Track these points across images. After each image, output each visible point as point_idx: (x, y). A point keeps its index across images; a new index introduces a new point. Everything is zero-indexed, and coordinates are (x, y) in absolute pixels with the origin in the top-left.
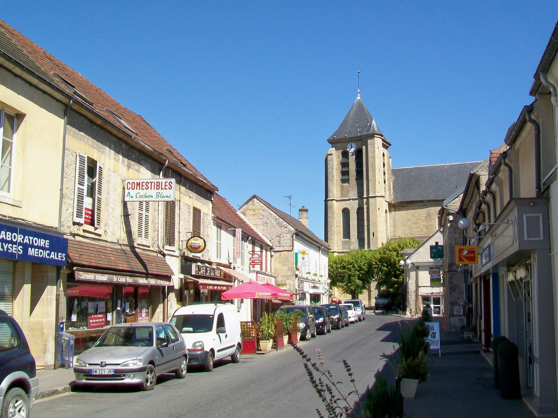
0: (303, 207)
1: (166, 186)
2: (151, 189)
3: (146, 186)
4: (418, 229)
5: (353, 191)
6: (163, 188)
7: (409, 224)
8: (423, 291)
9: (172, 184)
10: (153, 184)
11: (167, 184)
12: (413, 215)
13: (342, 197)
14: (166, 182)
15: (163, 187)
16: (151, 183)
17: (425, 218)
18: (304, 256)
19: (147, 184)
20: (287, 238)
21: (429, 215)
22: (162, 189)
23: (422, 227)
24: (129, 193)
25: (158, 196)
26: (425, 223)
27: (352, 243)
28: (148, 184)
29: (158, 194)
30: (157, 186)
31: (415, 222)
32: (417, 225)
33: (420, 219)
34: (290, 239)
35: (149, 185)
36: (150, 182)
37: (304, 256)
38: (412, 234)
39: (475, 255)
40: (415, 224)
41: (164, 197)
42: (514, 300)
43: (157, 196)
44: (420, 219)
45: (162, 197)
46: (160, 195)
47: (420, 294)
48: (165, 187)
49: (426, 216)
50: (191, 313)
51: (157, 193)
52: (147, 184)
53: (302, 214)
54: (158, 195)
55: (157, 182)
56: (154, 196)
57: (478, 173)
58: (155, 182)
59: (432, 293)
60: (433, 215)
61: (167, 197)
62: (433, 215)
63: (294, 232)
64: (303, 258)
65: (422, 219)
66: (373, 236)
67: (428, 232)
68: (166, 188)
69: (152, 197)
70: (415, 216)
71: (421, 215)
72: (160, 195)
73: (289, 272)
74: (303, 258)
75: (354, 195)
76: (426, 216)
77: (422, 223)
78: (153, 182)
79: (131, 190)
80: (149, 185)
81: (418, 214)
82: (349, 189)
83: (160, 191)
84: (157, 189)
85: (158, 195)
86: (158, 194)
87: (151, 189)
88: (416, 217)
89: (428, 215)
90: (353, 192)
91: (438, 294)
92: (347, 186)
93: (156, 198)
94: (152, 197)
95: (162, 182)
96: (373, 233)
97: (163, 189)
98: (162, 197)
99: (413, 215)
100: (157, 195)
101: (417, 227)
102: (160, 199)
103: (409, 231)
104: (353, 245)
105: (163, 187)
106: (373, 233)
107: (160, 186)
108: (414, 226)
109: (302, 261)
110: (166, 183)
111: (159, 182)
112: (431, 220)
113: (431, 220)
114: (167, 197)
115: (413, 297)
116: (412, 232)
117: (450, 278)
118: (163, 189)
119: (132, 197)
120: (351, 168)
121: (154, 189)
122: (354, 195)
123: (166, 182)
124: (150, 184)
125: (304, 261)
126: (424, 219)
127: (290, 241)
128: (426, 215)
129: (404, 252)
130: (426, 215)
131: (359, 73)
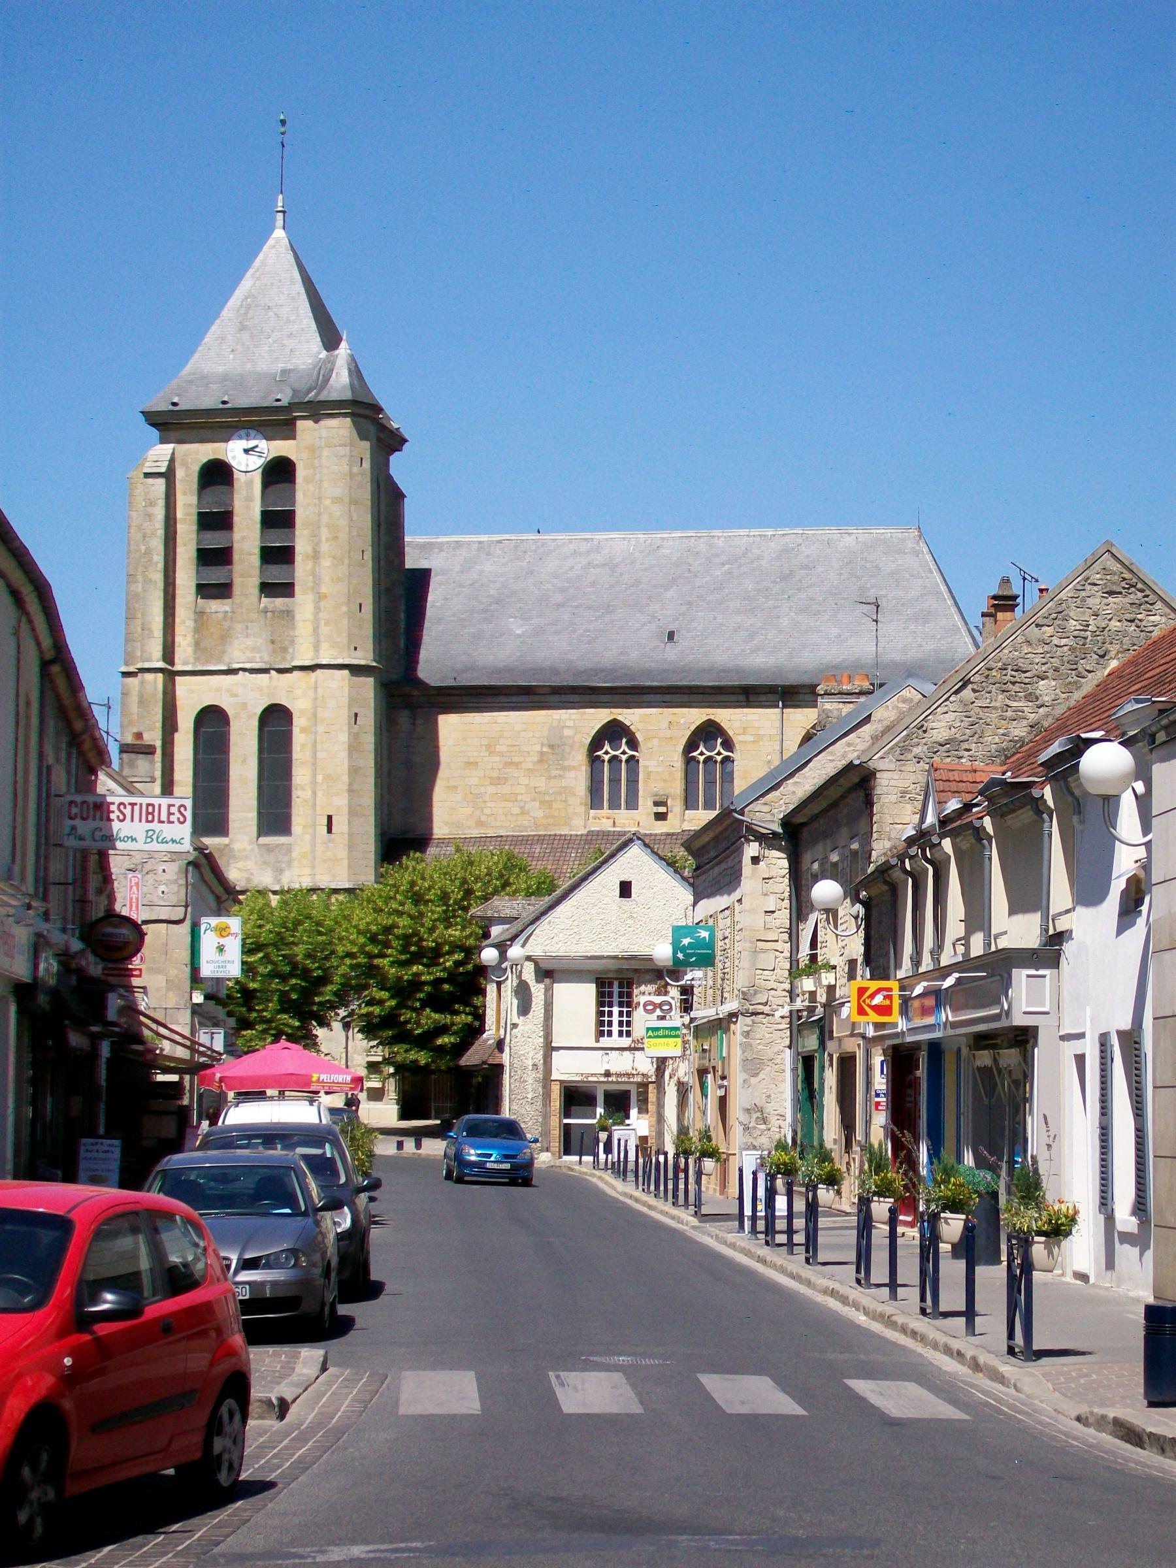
0: (139, 735)
1: (170, 814)
2: (132, 820)
3: (119, 814)
4: (509, 804)
5: (247, 636)
6: (162, 819)
7: (474, 781)
8: (568, 1068)
9: (186, 809)
10: (137, 808)
11: (173, 810)
12: (488, 746)
13: (197, 659)
14: (170, 806)
15: (164, 817)
16: (133, 805)
17: (541, 761)
18: (222, 941)
19: (122, 807)
20: (165, 877)
21: (556, 746)
22: (160, 822)
23: (526, 798)
24: (74, 828)
25: (149, 837)
26: (540, 783)
27: (234, 857)
28: (125, 808)
29: (151, 833)
30: (148, 813)
31: (495, 774)
32: (505, 789)
33: (516, 765)
34: (175, 881)
35: (128, 811)
36: (130, 804)
37: (222, 941)
38: (480, 824)
39: (891, 1002)
40: (497, 781)
41: (167, 842)
42: (986, 1101)
43: (149, 840)
44: (516, 765)
45: (160, 840)
46: (154, 837)
47: (555, 1075)
48: (169, 818)
49: (542, 753)
50: (269, 1121)
51: (147, 831)
52: (122, 807)
53: (132, 765)
54: (150, 837)
55: (148, 805)
56: (141, 837)
57: (872, 765)
58: (141, 805)
59: (607, 1074)
60: (571, 746)
61: (173, 841)
62: (571, 746)
63: (191, 858)
64: (221, 949)
65: (524, 766)
66: (330, 831)
67: (551, 820)
68: (171, 820)
69: (134, 839)
70: (498, 748)
71: (525, 748)
72: (154, 837)
73: (171, 994)
74: (221, 949)
75: (249, 654)
76: (542, 753)
77: (524, 781)
78: (136, 804)
79: (78, 822)
80: (128, 811)
81: (509, 742)
82: (230, 628)
83: (155, 825)
84: (147, 821)
85: (150, 837)
86: (151, 833)
87: (132, 820)
88: (501, 754)
89: (551, 747)
90: (249, 642)
91: (624, 1079)
92: (220, 616)
93: (145, 843)
94: (134, 839)
95: (160, 806)
96: (330, 818)
97: (163, 822)
98: (160, 840)
99: (488, 746)
100: (147, 837)
101: (505, 798)
102: (155, 846)
103: (469, 811)
104: (240, 865)
105: (164, 817)
106: (330, 818)
107: (156, 814)
108: (491, 790)
109: (217, 957)
110: (172, 808)
111: (153, 805)
112: (564, 768)
113: (564, 768)
114: (173, 841)
115: (530, 1088)
116: (483, 818)
117: (85, 893)
118: (163, 822)
119: (82, 839)
120: (243, 538)
121: (140, 821)
122: (249, 654)
123: (170, 806)
124: (129, 807)
125: (221, 958)
126: (535, 763)
127: (175, 888)
128: (545, 749)
129: (489, 913)
130: (545, 749)
131: (283, 122)
